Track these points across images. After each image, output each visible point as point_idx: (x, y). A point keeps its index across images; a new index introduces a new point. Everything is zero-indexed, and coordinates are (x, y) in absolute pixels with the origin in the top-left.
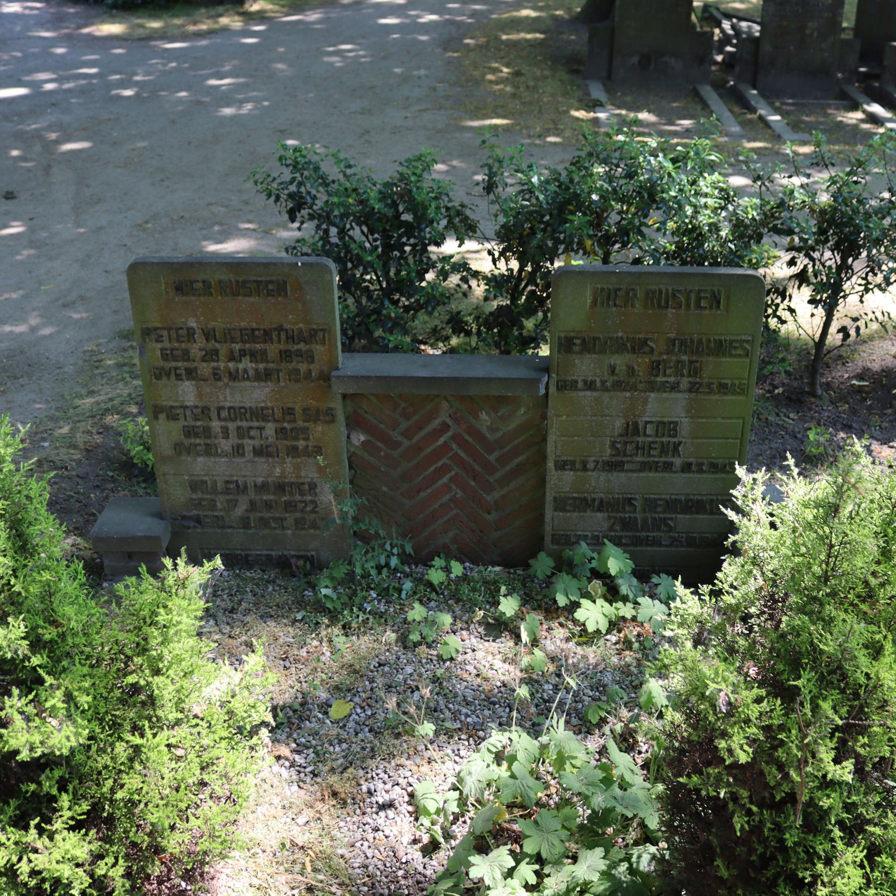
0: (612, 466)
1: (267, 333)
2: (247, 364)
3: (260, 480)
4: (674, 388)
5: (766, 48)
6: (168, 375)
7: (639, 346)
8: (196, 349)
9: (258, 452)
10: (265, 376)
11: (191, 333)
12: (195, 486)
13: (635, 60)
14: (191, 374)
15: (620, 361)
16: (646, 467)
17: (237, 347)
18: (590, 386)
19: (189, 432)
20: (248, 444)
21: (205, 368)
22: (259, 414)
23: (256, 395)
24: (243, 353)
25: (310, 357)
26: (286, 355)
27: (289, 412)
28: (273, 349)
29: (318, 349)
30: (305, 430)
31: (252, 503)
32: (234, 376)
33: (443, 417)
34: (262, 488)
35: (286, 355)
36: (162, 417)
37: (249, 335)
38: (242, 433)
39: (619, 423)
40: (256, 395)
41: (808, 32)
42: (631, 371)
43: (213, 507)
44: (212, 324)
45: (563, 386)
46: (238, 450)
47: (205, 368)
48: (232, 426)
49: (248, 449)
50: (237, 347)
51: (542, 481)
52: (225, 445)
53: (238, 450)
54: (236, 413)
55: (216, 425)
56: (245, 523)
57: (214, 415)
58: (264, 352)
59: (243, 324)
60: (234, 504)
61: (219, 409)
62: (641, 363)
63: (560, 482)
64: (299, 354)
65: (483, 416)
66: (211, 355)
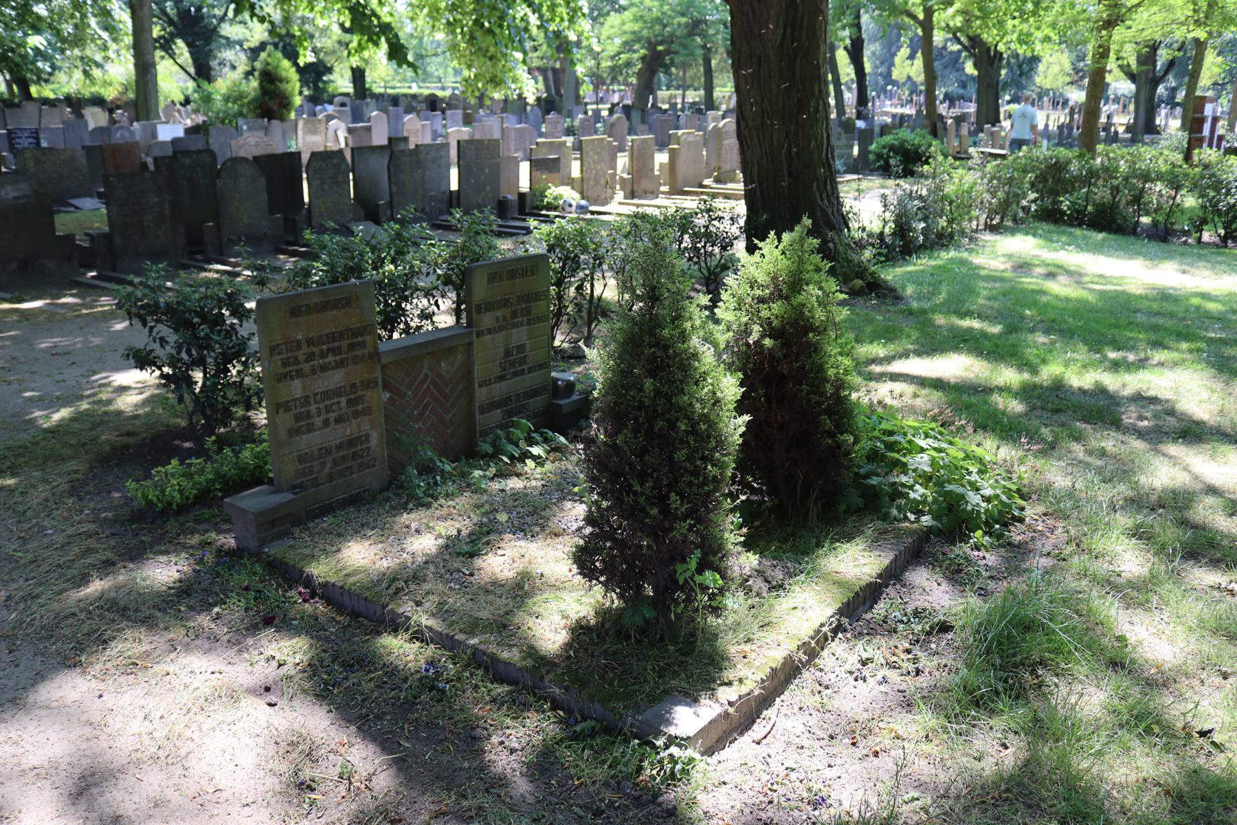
0: (502, 378)
1: (341, 333)
2: (331, 358)
3: (338, 441)
4: (522, 325)
5: (118, 240)
6: (285, 376)
7: (505, 303)
8: (301, 355)
9: (338, 420)
10: (340, 364)
11: (299, 343)
12: (301, 459)
13: (14, 265)
14: (299, 373)
15: (499, 313)
16: (516, 374)
17: (325, 347)
18: (490, 331)
19: (298, 418)
20: (332, 416)
21: (306, 367)
22: (337, 392)
23: (336, 378)
24: (329, 350)
25: (363, 345)
26: (351, 347)
27: (353, 386)
28: (344, 344)
29: (368, 338)
30: (361, 397)
31: (334, 460)
32: (323, 368)
33: (425, 371)
34: (340, 447)
35: (351, 347)
36: (281, 411)
37: (332, 337)
38: (328, 409)
39: (502, 350)
40: (336, 378)
41: (146, 224)
42: (505, 317)
43: (311, 472)
44: (311, 335)
45: (479, 334)
46: (326, 423)
47: (306, 367)
48: (322, 406)
49: (332, 420)
50: (325, 347)
51: (472, 397)
52: (318, 421)
53: (326, 423)
54: (327, 395)
55: (313, 408)
56: (330, 478)
57: (312, 401)
58: (340, 347)
59: (328, 331)
60: (323, 464)
61: (316, 394)
62: (507, 312)
63: (481, 394)
64: (359, 344)
65: (443, 364)
66: (310, 357)
